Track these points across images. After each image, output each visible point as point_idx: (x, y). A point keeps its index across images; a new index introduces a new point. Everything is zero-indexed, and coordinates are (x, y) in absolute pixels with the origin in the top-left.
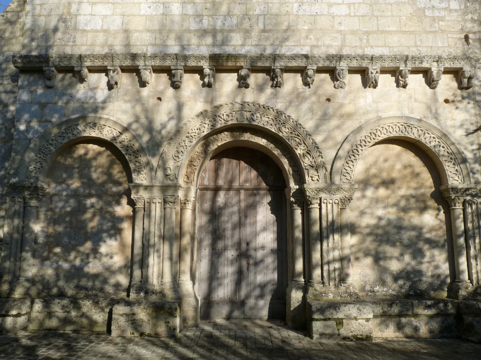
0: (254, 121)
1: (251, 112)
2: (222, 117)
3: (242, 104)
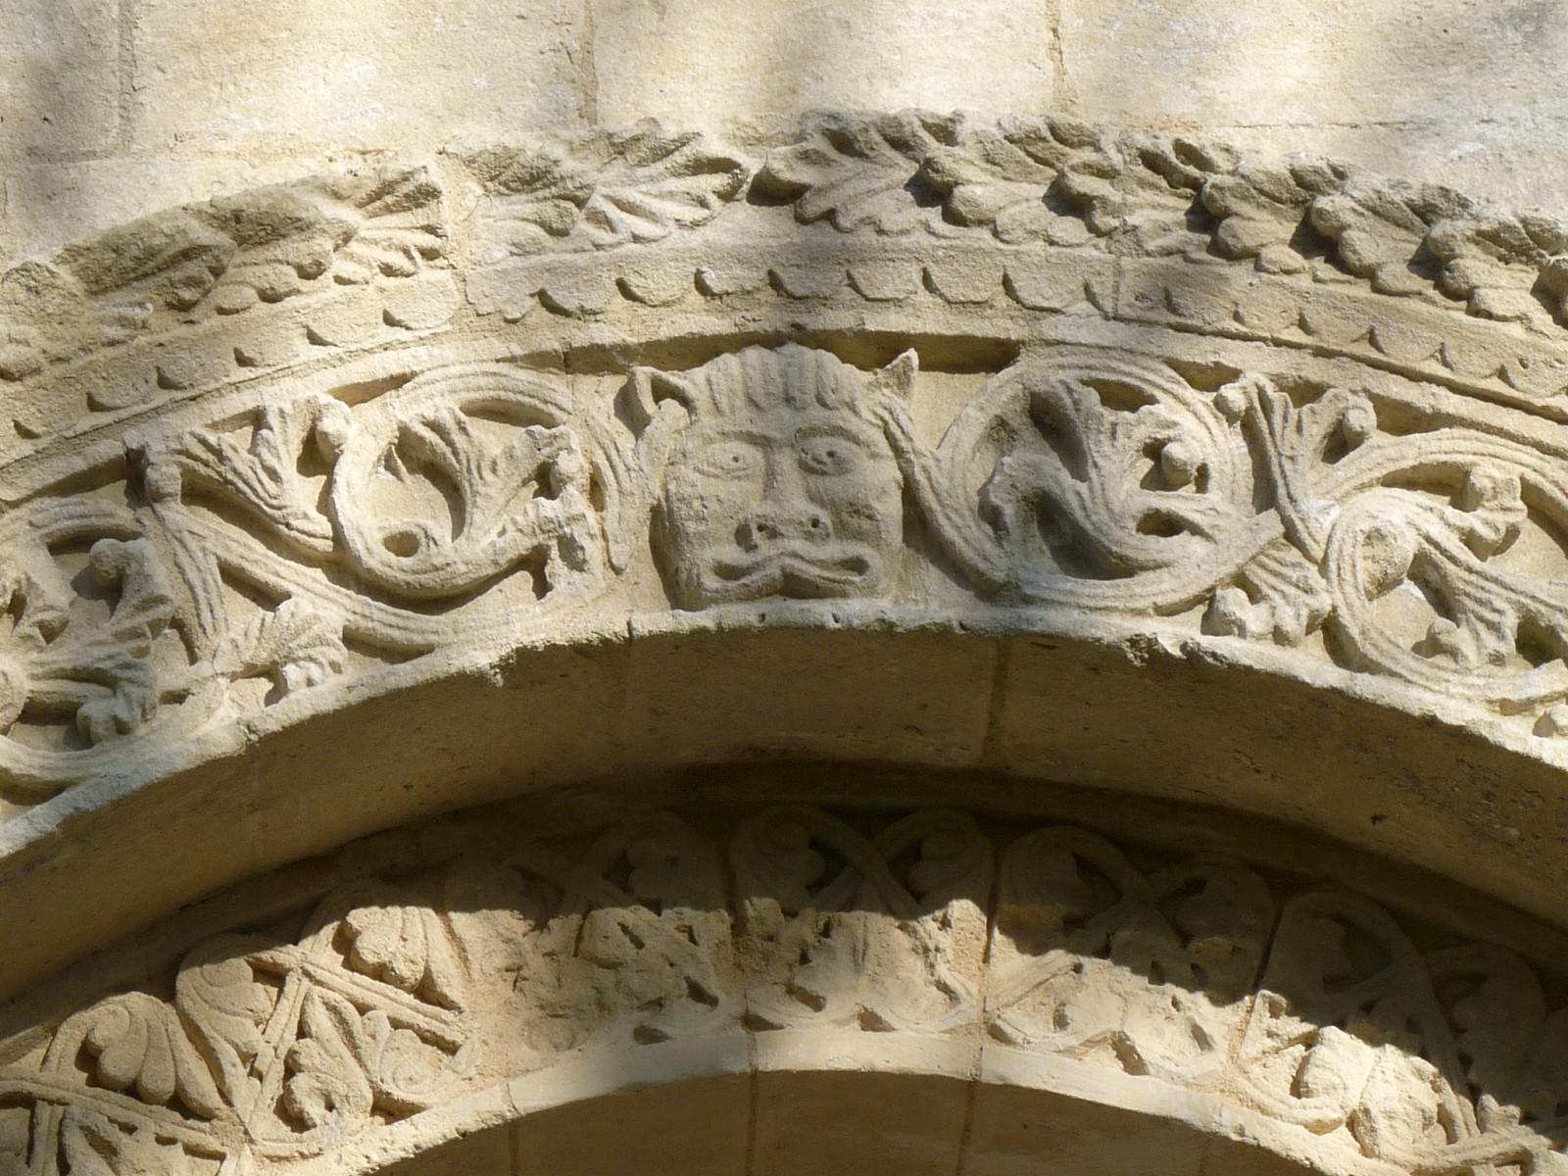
0: (1087, 556)
1: (994, 356)
2: (299, 494)
3: (768, 192)
